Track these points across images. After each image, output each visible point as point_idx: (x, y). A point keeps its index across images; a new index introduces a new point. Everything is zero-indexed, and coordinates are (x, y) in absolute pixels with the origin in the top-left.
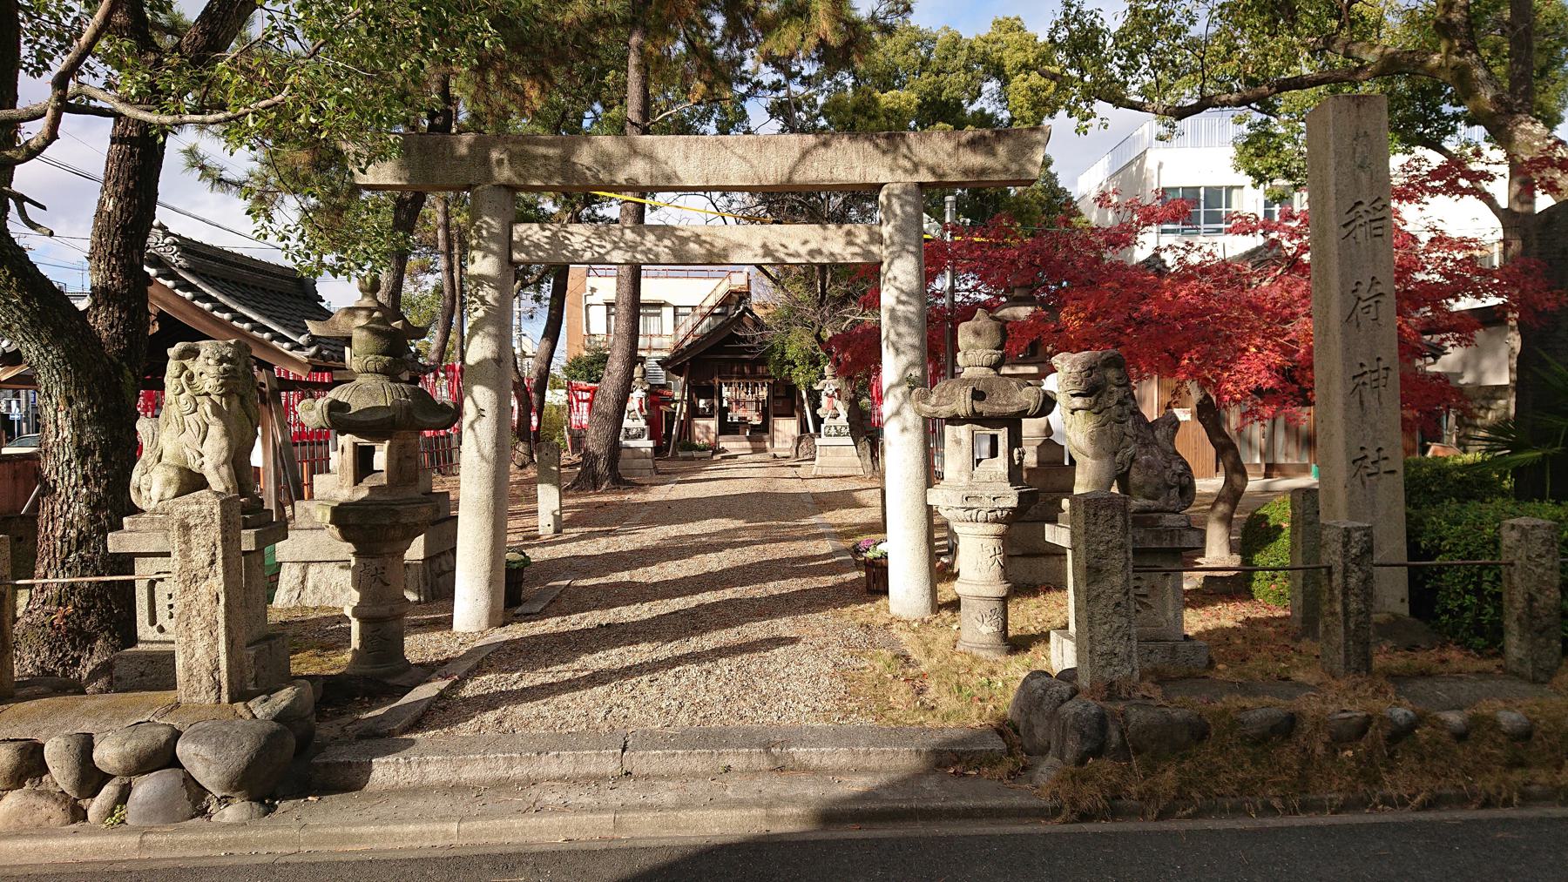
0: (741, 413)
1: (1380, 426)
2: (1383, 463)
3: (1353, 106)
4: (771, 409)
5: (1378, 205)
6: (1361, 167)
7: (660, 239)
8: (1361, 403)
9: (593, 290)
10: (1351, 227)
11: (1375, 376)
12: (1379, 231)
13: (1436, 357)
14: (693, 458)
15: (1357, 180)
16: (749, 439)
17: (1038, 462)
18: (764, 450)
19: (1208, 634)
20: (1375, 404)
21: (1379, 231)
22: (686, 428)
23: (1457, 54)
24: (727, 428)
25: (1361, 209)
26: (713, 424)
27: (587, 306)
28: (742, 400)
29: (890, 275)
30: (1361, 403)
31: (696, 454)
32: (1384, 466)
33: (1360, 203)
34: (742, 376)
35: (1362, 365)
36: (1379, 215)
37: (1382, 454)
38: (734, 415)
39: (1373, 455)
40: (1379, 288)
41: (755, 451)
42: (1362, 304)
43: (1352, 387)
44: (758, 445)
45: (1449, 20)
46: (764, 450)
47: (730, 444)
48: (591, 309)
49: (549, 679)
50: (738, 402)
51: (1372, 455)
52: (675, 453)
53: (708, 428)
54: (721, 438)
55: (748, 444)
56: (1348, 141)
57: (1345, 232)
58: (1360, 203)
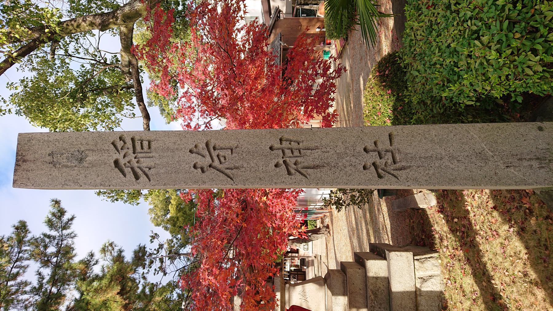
1: (341, 149)
2: (380, 147)
3: (25, 166)
5: (120, 144)
6: (81, 160)
8: (315, 167)
10: (138, 170)
11: (288, 152)
12: (145, 144)
13: (280, 11)
15: (93, 165)
16: (308, 267)
17: (344, 294)
18: (313, 261)
19: (536, 272)
20: (317, 154)
21: (145, 144)
23: (117, 20)
25: (122, 162)
30: (315, 167)
32: (384, 145)
33: (116, 163)
35: (277, 166)
36: (129, 144)
37: (371, 146)
39: (373, 157)
40: (202, 146)
41: (313, 265)
42: (216, 163)
43: (299, 176)
44: (310, 264)
45: (100, 24)
46: (313, 261)
51: (373, 157)
55: (310, 268)
56: (55, 172)
57: (143, 178)
58: (116, 163)
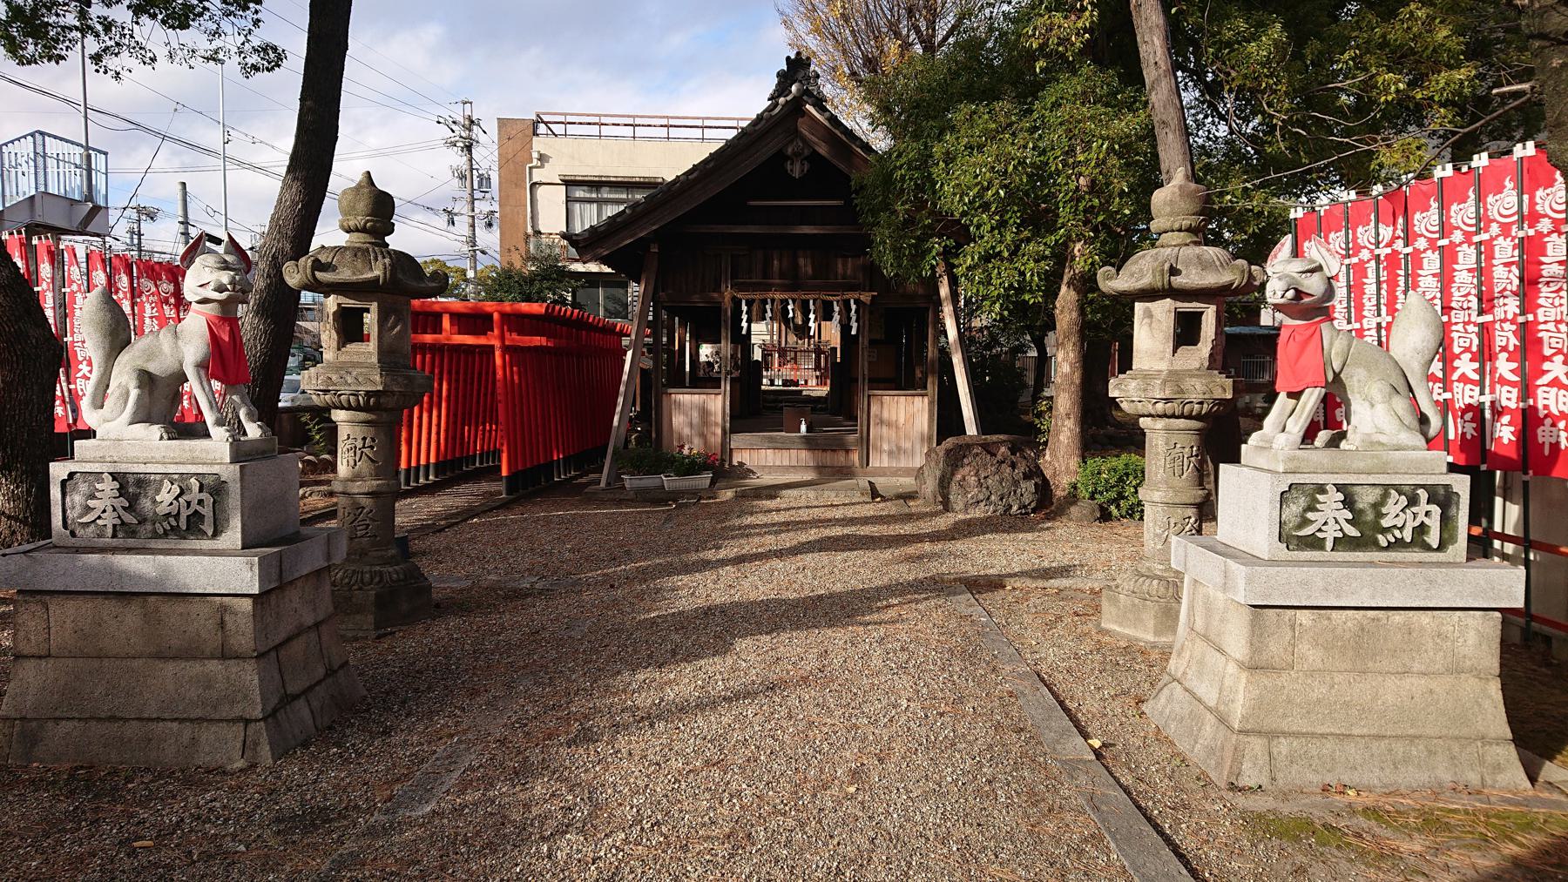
0: (788, 372)
4: (863, 367)
7: (1463, 747)
9: (543, 158)
14: (659, 497)
16: (810, 444)
22: (650, 414)
24: (756, 409)
26: (717, 403)
27: (533, 185)
28: (790, 342)
29: (1022, 545)
31: (669, 481)
34: (794, 283)
38: (773, 379)
46: (845, 472)
47: (768, 459)
48: (541, 191)
49: (915, 531)
50: (783, 352)
52: (616, 478)
53: (704, 412)
54: (737, 440)
55: (804, 455)
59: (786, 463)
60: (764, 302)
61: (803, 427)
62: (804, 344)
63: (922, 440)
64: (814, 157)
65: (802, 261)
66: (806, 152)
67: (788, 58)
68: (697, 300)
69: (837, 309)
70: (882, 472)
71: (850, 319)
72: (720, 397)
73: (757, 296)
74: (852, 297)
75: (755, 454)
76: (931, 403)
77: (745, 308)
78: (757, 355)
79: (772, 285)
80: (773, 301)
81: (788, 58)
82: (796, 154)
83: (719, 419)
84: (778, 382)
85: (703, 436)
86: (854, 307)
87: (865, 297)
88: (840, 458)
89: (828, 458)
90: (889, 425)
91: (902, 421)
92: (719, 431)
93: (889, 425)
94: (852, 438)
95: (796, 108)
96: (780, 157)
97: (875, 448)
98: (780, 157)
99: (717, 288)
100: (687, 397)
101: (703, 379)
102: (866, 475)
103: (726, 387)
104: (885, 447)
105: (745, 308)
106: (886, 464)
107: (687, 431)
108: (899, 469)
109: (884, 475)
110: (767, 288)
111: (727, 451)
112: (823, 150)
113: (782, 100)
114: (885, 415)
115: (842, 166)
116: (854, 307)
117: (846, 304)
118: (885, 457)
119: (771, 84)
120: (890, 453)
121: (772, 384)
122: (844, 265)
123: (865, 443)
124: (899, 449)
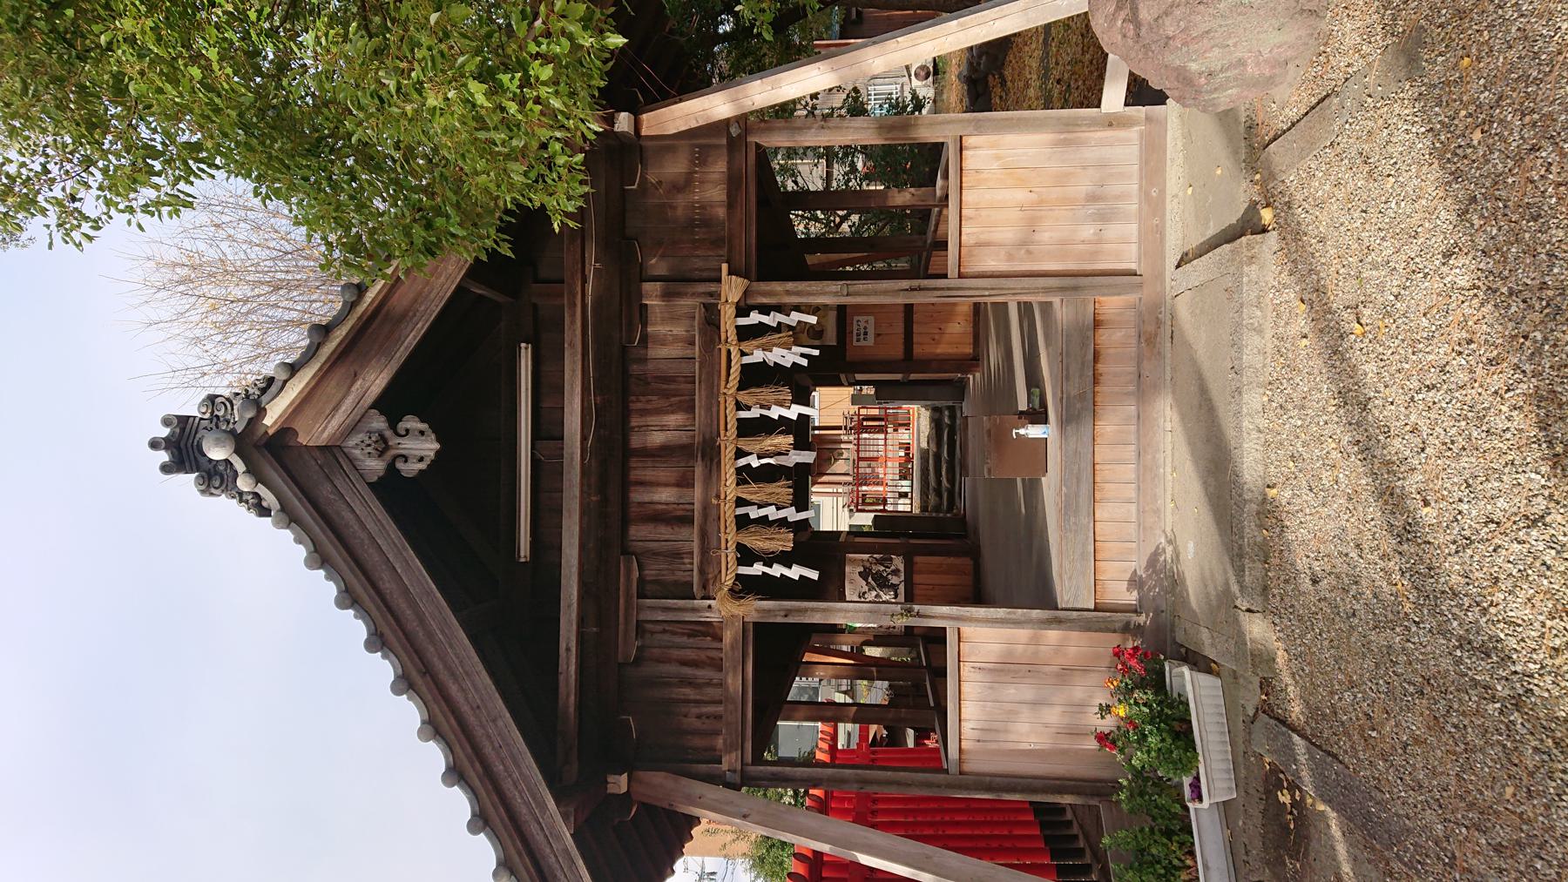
16: (1081, 410)
26: (980, 639)
31: (1215, 775)
50: (860, 480)
53: (1005, 669)
54: (1071, 588)
55: (1112, 424)
59: (1129, 471)
60: (743, 522)
61: (1034, 431)
62: (848, 450)
63: (1066, 143)
64: (391, 404)
65: (657, 439)
66: (379, 423)
67: (165, 469)
68: (737, 680)
69: (758, 356)
70: (1153, 236)
71: (780, 328)
72: (967, 630)
73: (730, 537)
74: (729, 321)
75: (1108, 549)
76: (979, 129)
77: (758, 569)
78: (865, 519)
79: (706, 507)
80: (740, 502)
81: (165, 469)
82: (383, 446)
83: (1023, 634)
84: (905, 486)
85: (1066, 674)
86: (755, 318)
87: (732, 289)
88: (1114, 340)
89: (1115, 369)
90: (1032, 225)
91: (1020, 195)
92: (1053, 635)
93: (1032, 225)
94: (1063, 311)
95: (249, 443)
96: (391, 488)
97: (1094, 255)
98: (391, 488)
99: (710, 631)
100: (969, 710)
101: (919, 675)
102: (1160, 277)
103: (939, 615)
104: (1088, 231)
105: (758, 569)
106: (1132, 229)
107: (1053, 716)
108: (1145, 195)
109: (1160, 231)
110: (710, 513)
111: (1100, 617)
112: (375, 381)
113: (244, 484)
114: (1007, 235)
115: (412, 338)
116: (755, 318)
117: (745, 334)
118: (1113, 230)
119: (224, 506)
120: (1104, 218)
121: (903, 495)
122: (663, 342)
123: (1074, 280)
124: (1093, 198)
